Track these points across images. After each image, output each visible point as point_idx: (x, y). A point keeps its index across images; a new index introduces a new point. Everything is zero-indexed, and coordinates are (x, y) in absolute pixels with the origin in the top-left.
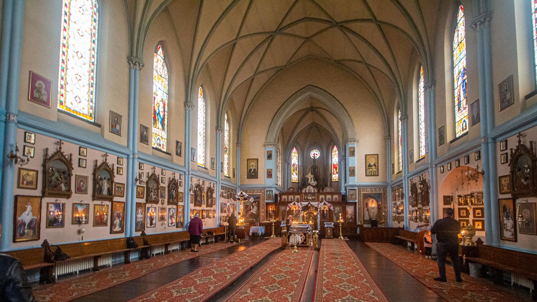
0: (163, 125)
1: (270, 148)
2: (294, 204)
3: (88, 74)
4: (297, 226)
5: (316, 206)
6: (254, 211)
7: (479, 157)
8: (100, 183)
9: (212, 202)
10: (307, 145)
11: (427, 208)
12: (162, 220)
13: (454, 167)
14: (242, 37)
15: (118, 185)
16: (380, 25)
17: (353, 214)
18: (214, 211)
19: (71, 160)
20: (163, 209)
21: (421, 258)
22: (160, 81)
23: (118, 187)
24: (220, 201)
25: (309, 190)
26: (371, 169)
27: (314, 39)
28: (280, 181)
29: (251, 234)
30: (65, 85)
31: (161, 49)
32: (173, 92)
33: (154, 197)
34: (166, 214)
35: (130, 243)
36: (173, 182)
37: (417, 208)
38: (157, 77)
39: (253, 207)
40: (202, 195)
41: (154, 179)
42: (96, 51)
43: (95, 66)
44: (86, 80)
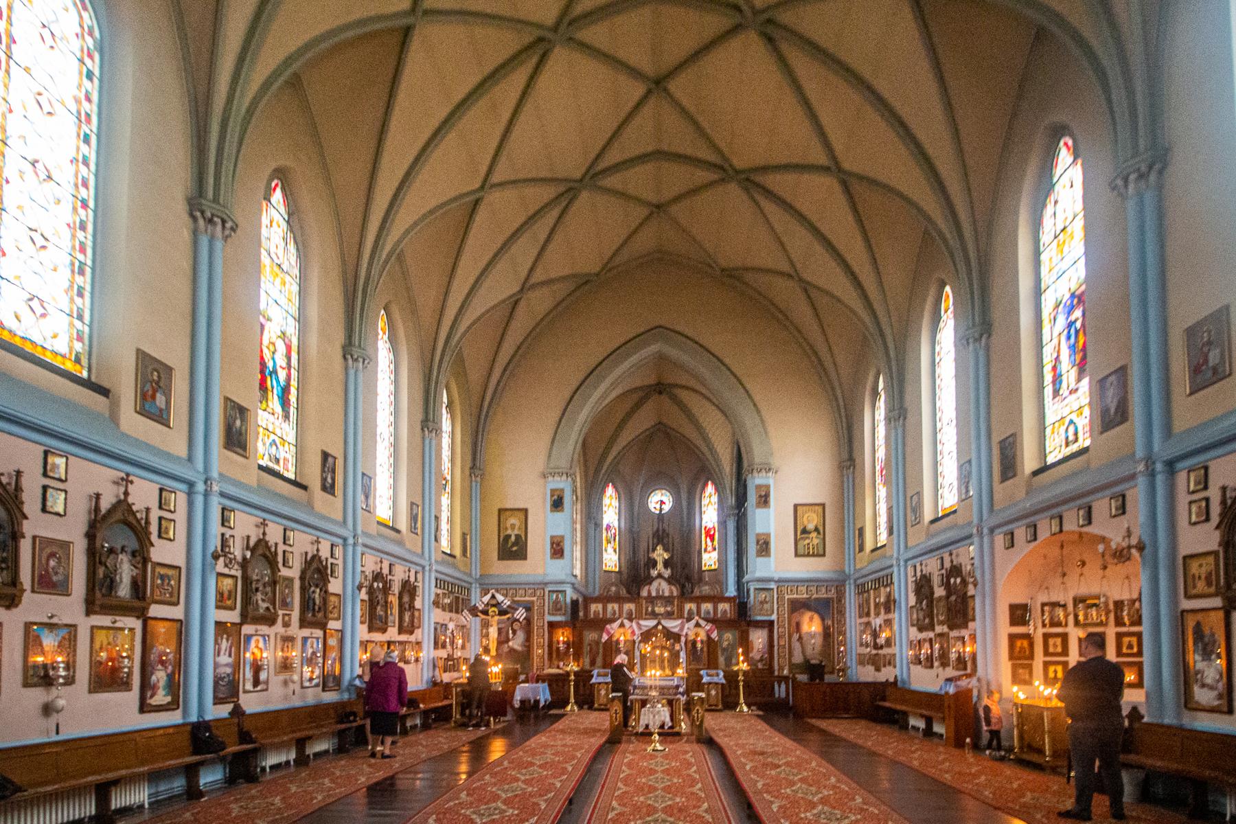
0: (285, 403)
1: (562, 483)
2: (622, 625)
3: (67, 233)
4: (658, 683)
5: (676, 630)
6: (516, 643)
7: (1122, 510)
8: (110, 562)
9: (412, 621)
11: (965, 633)
12: (285, 669)
13: (1043, 534)
14: (501, 184)
15: (163, 571)
16: (847, 181)
18: (418, 643)
19: (18, 488)
20: (288, 640)
21: (970, 756)
22: (279, 285)
23: (162, 577)
24: (431, 617)
25: (658, 591)
26: (806, 540)
27: (674, 209)
28: (578, 566)
29: (517, 705)
31: (278, 190)
34: (295, 653)
35: (201, 738)
36: (314, 565)
37: (931, 635)
38: (268, 268)
39: (514, 632)
40: (387, 602)
41: (264, 556)
42: (93, 167)
43: (91, 213)
44: (60, 254)
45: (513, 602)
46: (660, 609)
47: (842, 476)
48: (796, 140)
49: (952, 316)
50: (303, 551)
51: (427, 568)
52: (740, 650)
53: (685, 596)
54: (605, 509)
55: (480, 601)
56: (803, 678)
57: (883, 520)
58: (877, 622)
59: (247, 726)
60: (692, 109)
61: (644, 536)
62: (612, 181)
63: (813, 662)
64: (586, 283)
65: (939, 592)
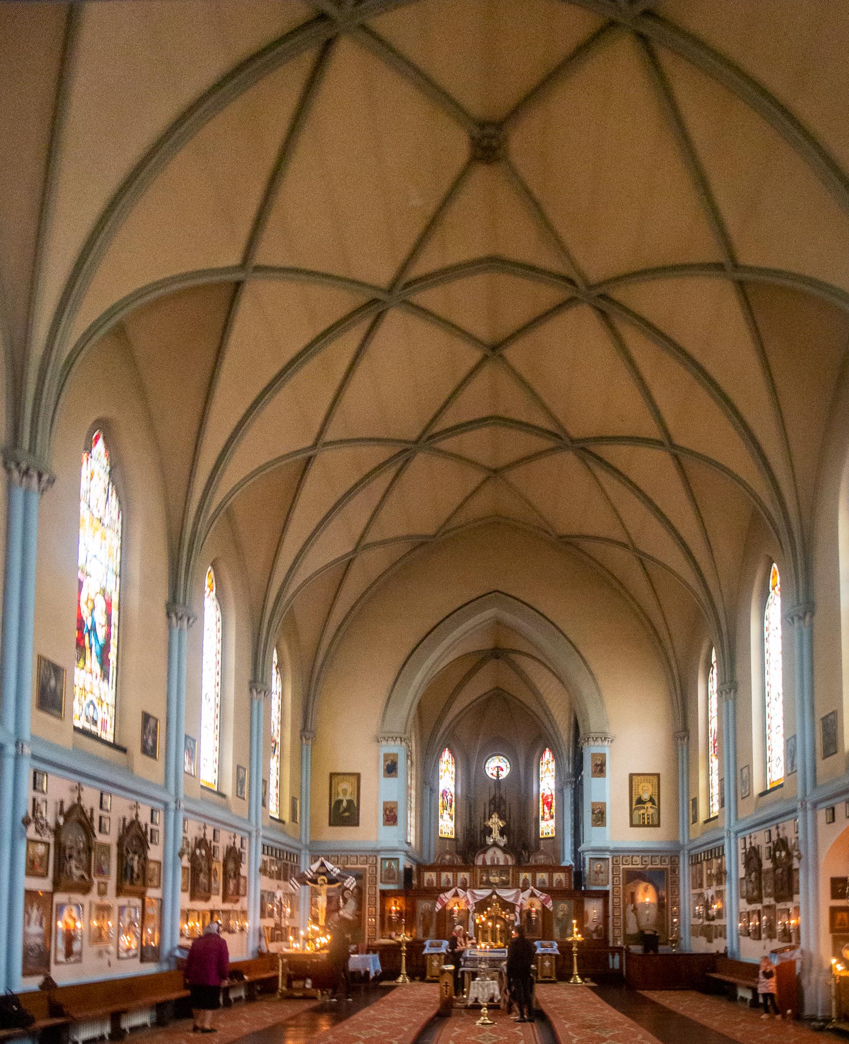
2: (456, 895)
4: (488, 955)
5: (510, 900)
6: (348, 911)
10: (478, 747)
11: (790, 905)
17: (601, 920)
20: (103, 910)
21: (791, 1028)
24: (257, 884)
25: (492, 859)
26: (642, 810)
27: (514, 476)
28: (413, 833)
31: (101, 442)
32: (136, 573)
33: (77, 873)
36: (133, 831)
37: (759, 907)
39: (345, 901)
40: (211, 868)
41: (80, 822)
45: (344, 870)
47: (677, 745)
48: (631, 415)
49: (779, 593)
50: (121, 815)
51: (254, 834)
52: (574, 921)
53: (520, 866)
54: (441, 774)
55: (310, 868)
56: (637, 949)
57: (715, 790)
58: (709, 893)
59: (59, 998)
60: (527, 377)
61: (479, 801)
62: (447, 444)
63: (647, 932)
65: (767, 865)
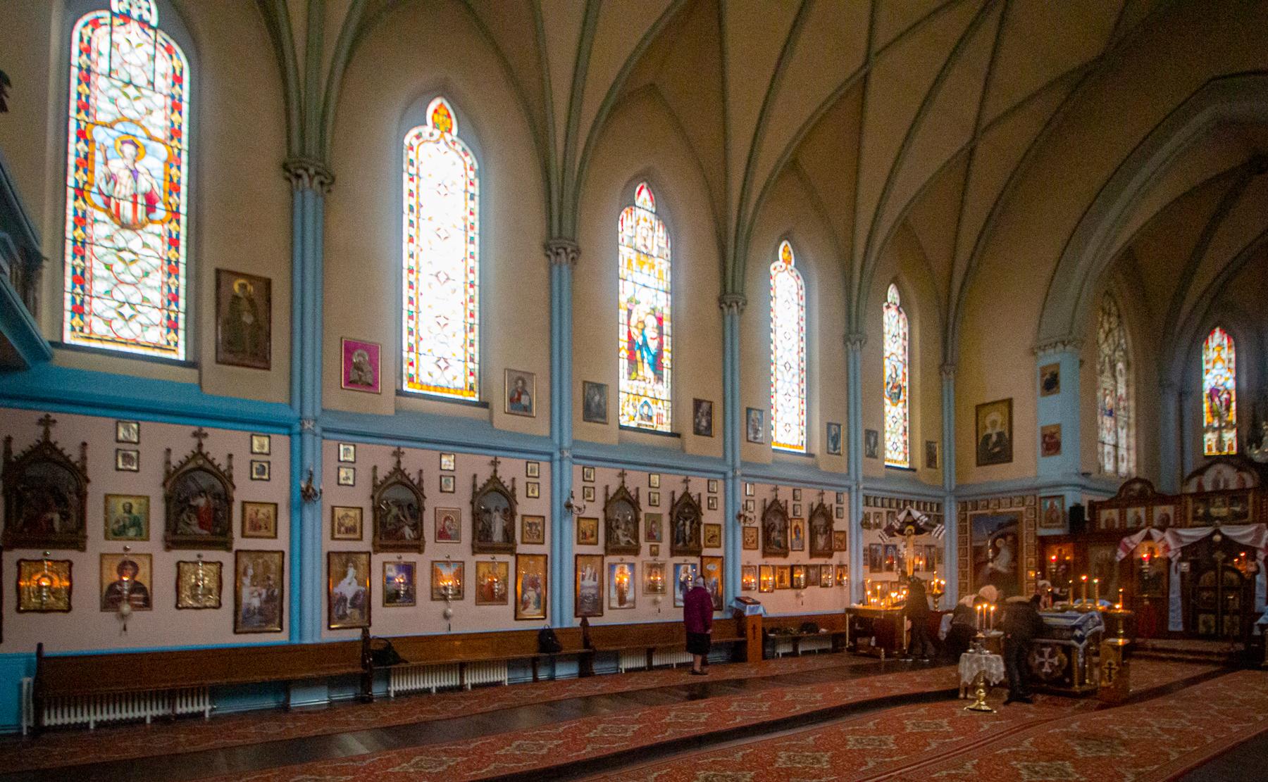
1: (1050, 358)
2: (1148, 537)
3: (462, 307)
12: (641, 591)
15: (530, 520)
23: (530, 525)
25: (1216, 482)
29: (943, 636)
30: (417, 343)
33: (623, 540)
39: (997, 551)
46: (1219, 510)
51: (854, 488)
64: (1087, 75)
